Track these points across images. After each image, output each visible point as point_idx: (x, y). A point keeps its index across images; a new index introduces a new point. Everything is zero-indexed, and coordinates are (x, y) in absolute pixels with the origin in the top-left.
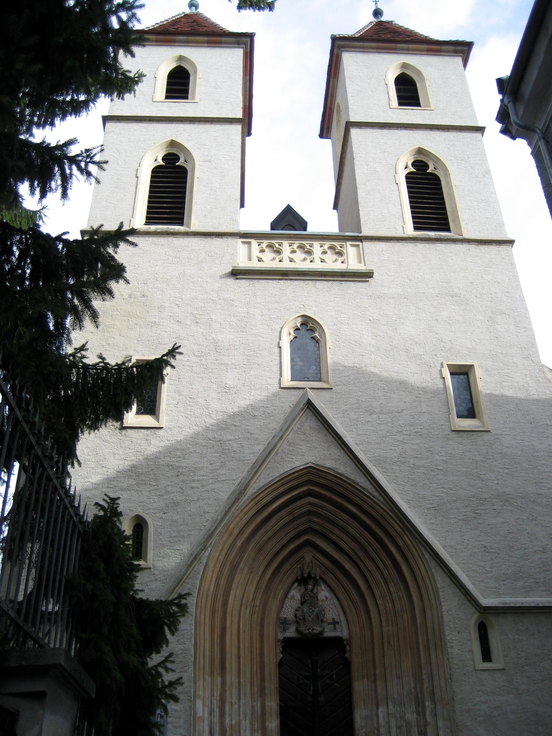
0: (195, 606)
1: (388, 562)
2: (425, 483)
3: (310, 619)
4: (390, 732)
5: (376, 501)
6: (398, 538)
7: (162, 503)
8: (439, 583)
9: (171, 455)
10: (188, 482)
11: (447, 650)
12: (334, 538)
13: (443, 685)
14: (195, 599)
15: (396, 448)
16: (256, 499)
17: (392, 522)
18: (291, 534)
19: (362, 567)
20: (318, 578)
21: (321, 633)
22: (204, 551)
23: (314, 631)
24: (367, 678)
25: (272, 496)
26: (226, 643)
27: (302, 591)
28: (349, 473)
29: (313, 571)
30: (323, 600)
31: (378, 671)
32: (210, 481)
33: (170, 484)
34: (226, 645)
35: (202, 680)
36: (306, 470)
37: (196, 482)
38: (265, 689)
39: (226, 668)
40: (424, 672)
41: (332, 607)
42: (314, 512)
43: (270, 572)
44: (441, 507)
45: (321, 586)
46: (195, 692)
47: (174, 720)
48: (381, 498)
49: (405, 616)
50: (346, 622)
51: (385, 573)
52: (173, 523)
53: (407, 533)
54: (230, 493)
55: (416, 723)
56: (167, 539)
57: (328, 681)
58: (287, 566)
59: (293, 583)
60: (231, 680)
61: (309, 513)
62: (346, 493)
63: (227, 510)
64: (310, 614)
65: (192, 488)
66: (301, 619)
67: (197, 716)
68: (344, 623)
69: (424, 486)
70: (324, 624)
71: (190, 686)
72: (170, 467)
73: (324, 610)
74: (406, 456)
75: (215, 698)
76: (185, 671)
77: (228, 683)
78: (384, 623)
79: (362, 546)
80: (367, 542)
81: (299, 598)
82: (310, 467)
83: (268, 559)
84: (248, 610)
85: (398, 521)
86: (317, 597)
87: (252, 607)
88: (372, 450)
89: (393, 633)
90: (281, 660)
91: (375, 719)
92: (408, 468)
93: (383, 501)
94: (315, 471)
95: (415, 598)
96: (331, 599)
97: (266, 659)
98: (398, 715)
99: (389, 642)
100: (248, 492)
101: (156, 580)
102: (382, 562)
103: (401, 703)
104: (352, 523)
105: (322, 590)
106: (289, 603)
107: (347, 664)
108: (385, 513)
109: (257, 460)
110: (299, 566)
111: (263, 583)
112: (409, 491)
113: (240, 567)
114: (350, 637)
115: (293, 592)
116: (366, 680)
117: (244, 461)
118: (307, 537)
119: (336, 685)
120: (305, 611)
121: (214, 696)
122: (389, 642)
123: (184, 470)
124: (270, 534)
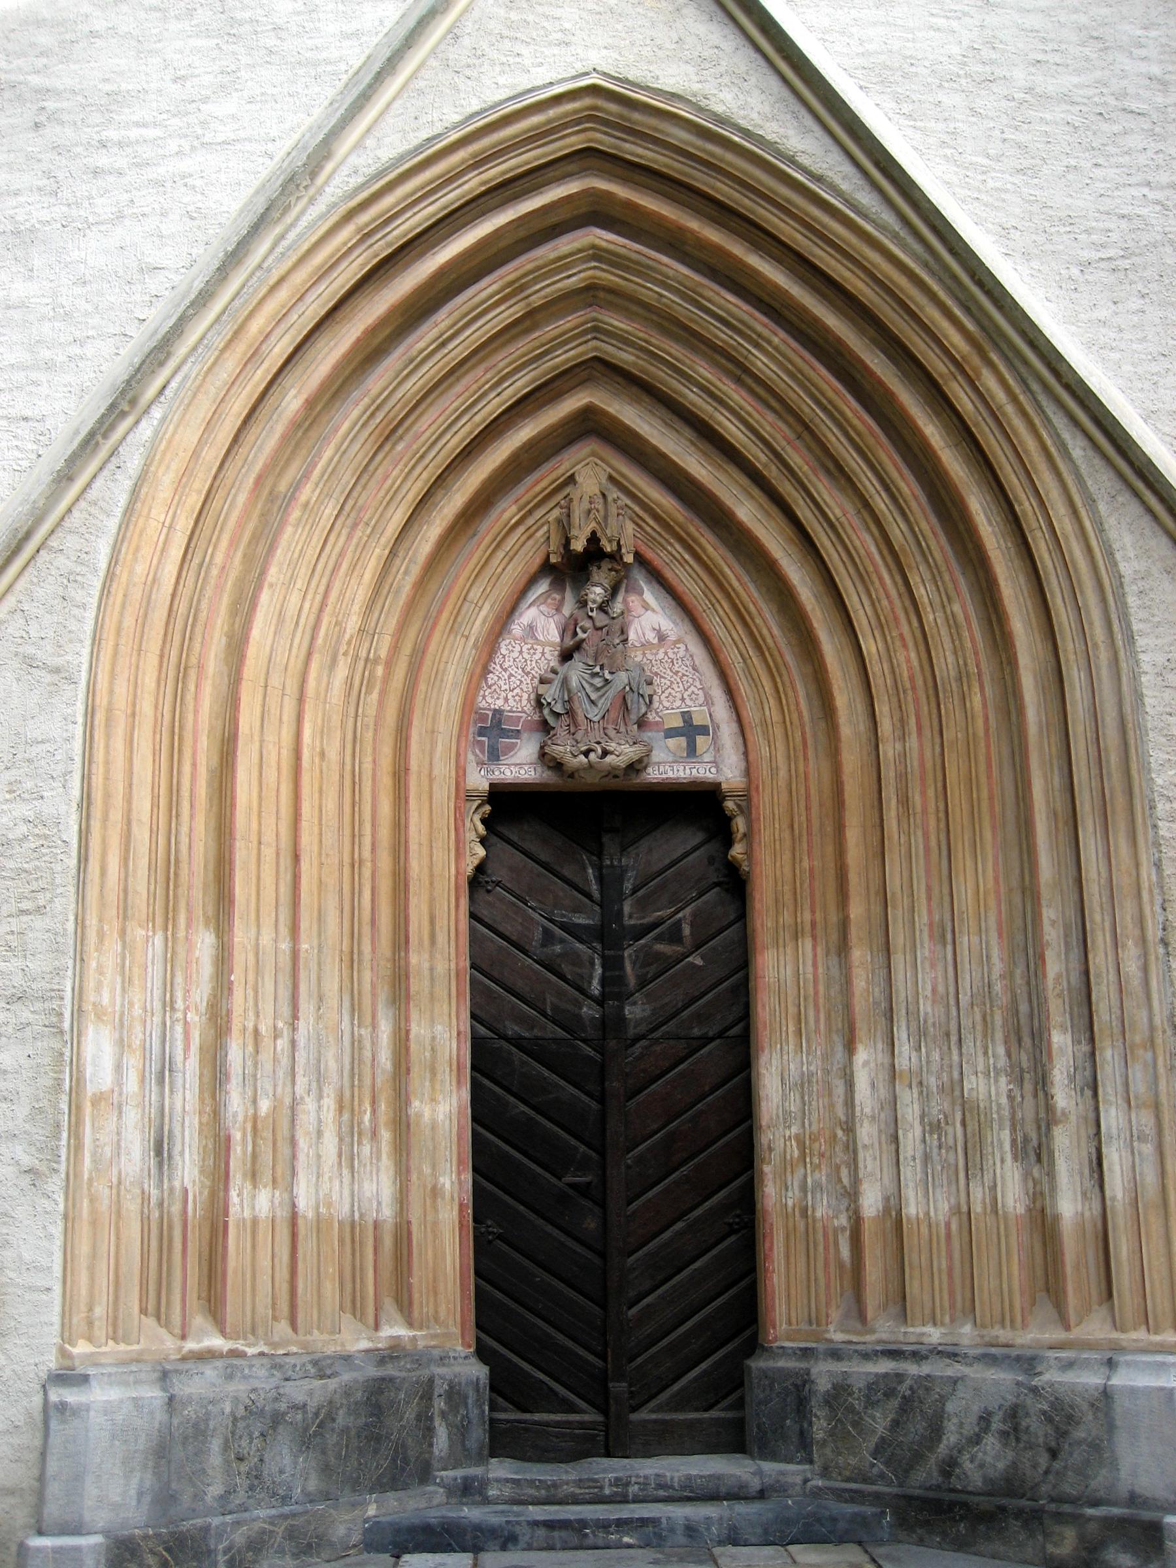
0: (88, 642)
1: (908, 486)
2: (1073, 162)
3: (594, 714)
4: (895, 1139)
5: (869, 228)
6: (955, 385)
10: (79, 149)
11: (1155, 826)
12: (692, 398)
13: (1131, 967)
14: (90, 615)
15: (954, 24)
16: (364, 218)
17: (932, 314)
18: (521, 384)
19: (804, 512)
20: (629, 558)
21: (636, 767)
24: (814, 938)
25: (431, 209)
28: (755, 116)
30: (646, 645)
31: (856, 910)
32: (173, 146)
34: (233, 806)
35: (113, 945)
36: (576, 105)
37: (115, 150)
38: (407, 977)
39: (232, 902)
40: (1049, 914)
42: (612, 291)
44: (1137, 260)
45: (641, 593)
46: (79, 993)
48: (888, 218)
49: (977, 699)
50: (734, 726)
51: (897, 531)
52: (12, 312)
53: (994, 357)
54: (251, 191)
55: (1006, 1113)
57: (660, 947)
58: (507, 510)
59: (532, 581)
60: (257, 945)
61: (590, 294)
63: (230, 249)
64: (594, 696)
65: (96, 172)
66: (557, 715)
67: (90, 1090)
68: (727, 732)
69: (1070, 177)
71: (58, 972)
73: (650, 683)
75: (179, 1015)
76: (39, 910)
77: (241, 958)
78: (886, 726)
79: (805, 429)
80: (824, 409)
81: (554, 635)
82: (594, 90)
83: (425, 475)
84: (342, 672)
85: (958, 312)
86: (623, 631)
87: (361, 664)
88: (854, 30)
89: (922, 764)
90: (480, 869)
91: (840, 1090)
92: (1004, 104)
93: (896, 226)
94: (613, 107)
96: (679, 641)
98: (933, 1080)
99: (905, 801)
102: (887, 489)
103: (948, 1035)
104: (766, 333)
105: (646, 607)
106: (516, 654)
108: (903, 281)
109: (368, 57)
110: (556, 513)
111: (406, 573)
112: (1006, 191)
114: (749, 782)
115: (529, 615)
116: (808, 943)
117: (316, 64)
119: (690, 959)
120: (574, 682)
121: (173, 1009)
122: (905, 801)
123: (65, 104)
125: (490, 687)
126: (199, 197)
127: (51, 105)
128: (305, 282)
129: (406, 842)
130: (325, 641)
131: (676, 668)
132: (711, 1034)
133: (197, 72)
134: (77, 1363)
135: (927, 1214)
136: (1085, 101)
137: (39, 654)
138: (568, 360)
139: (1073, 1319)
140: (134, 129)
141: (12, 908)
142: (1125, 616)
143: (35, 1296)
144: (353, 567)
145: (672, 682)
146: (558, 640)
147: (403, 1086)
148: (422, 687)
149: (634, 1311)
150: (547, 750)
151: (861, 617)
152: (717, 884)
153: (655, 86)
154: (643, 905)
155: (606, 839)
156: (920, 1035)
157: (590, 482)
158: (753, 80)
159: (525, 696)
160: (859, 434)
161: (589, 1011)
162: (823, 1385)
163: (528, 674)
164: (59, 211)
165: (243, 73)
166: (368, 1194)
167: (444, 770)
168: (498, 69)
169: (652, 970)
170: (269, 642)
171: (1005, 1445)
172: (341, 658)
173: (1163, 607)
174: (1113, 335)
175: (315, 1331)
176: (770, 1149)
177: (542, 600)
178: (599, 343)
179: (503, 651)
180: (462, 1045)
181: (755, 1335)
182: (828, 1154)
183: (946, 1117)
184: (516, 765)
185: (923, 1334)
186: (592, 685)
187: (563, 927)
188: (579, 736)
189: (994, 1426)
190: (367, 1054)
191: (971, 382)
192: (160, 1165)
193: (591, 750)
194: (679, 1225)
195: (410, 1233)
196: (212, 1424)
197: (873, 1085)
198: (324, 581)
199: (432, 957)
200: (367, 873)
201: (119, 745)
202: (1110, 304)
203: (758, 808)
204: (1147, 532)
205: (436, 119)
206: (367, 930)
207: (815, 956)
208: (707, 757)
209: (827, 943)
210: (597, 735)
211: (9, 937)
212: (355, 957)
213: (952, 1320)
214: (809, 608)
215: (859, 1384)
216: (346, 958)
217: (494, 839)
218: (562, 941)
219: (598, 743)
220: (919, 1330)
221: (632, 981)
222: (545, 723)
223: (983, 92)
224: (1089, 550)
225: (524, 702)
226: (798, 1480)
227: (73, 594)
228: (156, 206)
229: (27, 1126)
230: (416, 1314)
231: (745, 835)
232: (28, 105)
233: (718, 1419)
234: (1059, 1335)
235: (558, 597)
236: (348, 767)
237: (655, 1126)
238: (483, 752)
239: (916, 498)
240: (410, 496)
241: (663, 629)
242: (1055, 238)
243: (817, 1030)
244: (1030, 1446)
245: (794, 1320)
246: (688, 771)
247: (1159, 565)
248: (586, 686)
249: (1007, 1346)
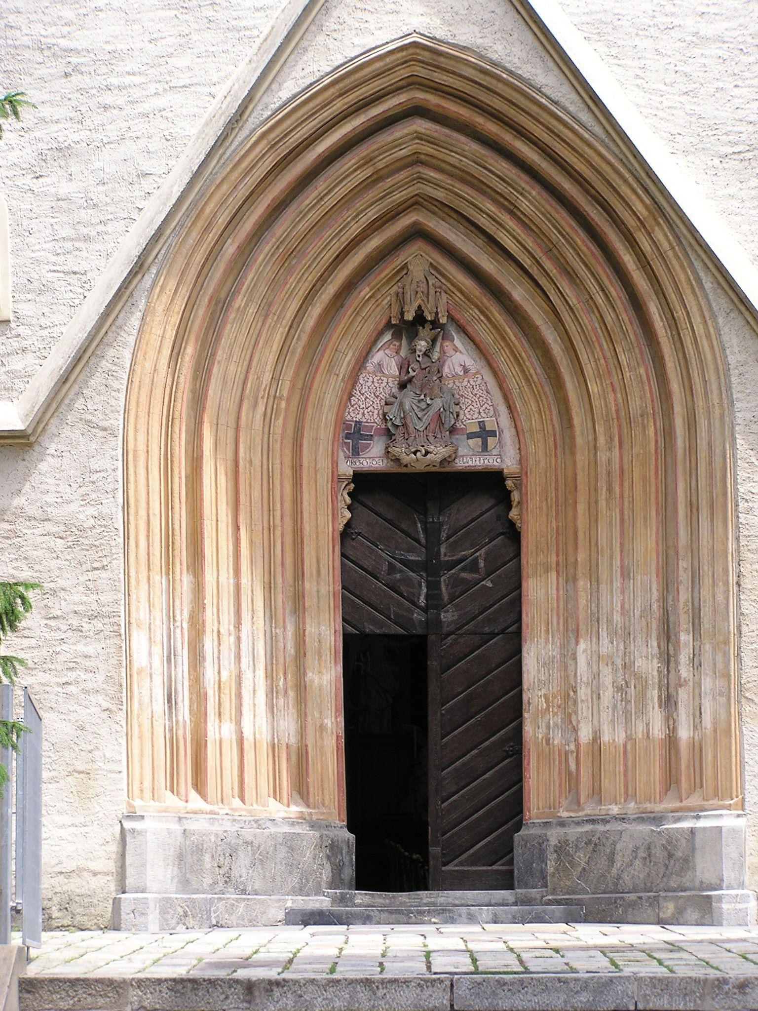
1: (616, 291)
2: (721, 85)
3: (420, 426)
7: (29, 151)
8: (733, 353)
9: (45, 19)
10: (94, 91)
11: (738, 516)
12: (482, 221)
14: (122, 396)
16: (272, 136)
17: (624, 190)
18: (372, 214)
22: (140, 276)
23: (429, 456)
24: (558, 573)
25: (313, 123)
26: (202, 495)
27: (403, 353)
28: (516, 60)
30: (455, 376)
33: (47, 97)
35: (144, 586)
37: (116, 92)
39: (203, 557)
43: (316, 311)
47: (83, 677)
48: (597, 130)
52: (61, 203)
56: (46, 246)
57: (464, 575)
58: (365, 291)
59: (381, 333)
61: (416, 160)
62: (512, 113)
65: (106, 108)
68: (508, 435)
69: (717, 95)
70: (460, 438)
72: (46, 53)
74: (674, 10)
78: (602, 441)
80: (564, 237)
82: (414, 44)
84: (261, 409)
90: (348, 525)
92: (680, 45)
95: (675, 386)
96: (477, 373)
97: (308, 528)
100: (249, 116)
101: (24, 350)
102: (603, 290)
105: (456, 350)
106: (369, 384)
107: (514, 535)
110: (395, 288)
111: (298, 339)
112: (676, 108)
113: (237, 306)
115: (378, 357)
116: (554, 575)
118: (414, 219)
120: (407, 407)
124: (313, 216)
125: (352, 406)
126: (171, 125)
127: (74, 60)
128: (237, 178)
129: (302, 512)
130: (250, 391)
131: (475, 392)
132: (496, 631)
133: (163, 35)
134: (137, 810)
135: (614, 740)
136: (732, 40)
137: (94, 419)
138: (401, 197)
139: (684, 795)
140: (127, 76)
141: (88, 566)
142: (729, 388)
143: (114, 775)
144: (266, 342)
146: (398, 373)
147: (302, 664)
148: (310, 411)
149: (445, 804)
150: (390, 450)
151: (589, 370)
152: (502, 534)
153: (453, 41)
154: (453, 547)
155: (429, 504)
156: (613, 634)
157: (418, 270)
158: (516, 36)
159: (376, 412)
160: (585, 256)
161: (418, 616)
162: (553, 841)
163: (377, 397)
164: (84, 134)
165: (193, 35)
166: (282, 728)
167: (324, 464)
168: (354, 32)
169: (458, 590)
170: (219, 396)
171: (644, 865)
172: (260, 400)
173: (753, 383)
174: (738, 205)
175: (255, 805)
176: (529, 703)
177: (386, 346)
178: (422, 185)
179: (361, 381)
180: (338, 638)
181: (521, 820)
182: (563, 706)
183: (626, 683)
185: (609, 809)
187: (402, 562)
188: (410, 442)
189: (639, 855)
190: (281, 645)
191: (649, 234)
192: (170, 708)
193: (418, 451)
194: (475, 751)
195: (307, 753)
196: (205, 846)
197: (588, 664)
198: (249, 352)
199: (318, 583)
200: (278, 534)
201: (142, 472)
202: (738, 183)
203: (526, 487)
204: (748, 336)
205: (315, 70)
206: (279, 569)
207: (558, 583)
208: (494, 452)
209: (567, 575)
210: (422, 440)
211: (88, 583)
212: (272, 585)
213: (625, 801)
214: (558, 359)
215: (572, 839)
216: (267, 586)
217: (357, 505)
218: (401, 571)
220: (607, 807)
221: (446, 597)
222: (388, 430)
223: (665, 37)
224: (712, 347)
225: (375, 416)
226: (538, 896)
227: (112, 383)
228: (145, 131)
229: (104, 686)
230: (311, 800)
231: (519, 502)
232: (60, 60)
233: (496, 871)
234: (678, 804)
235: (397, 344)
236: (265, 467)
237: (460, 690)
238: (348, 450)
239: (620, 298)
240: (301, 292)
242: (706, 140)
243: (558, 629)
244: (655, 864)
245: (541, 806)
246: (482, 461)
247: (753, 357)
248: (415, 408)
249: (651, 812)
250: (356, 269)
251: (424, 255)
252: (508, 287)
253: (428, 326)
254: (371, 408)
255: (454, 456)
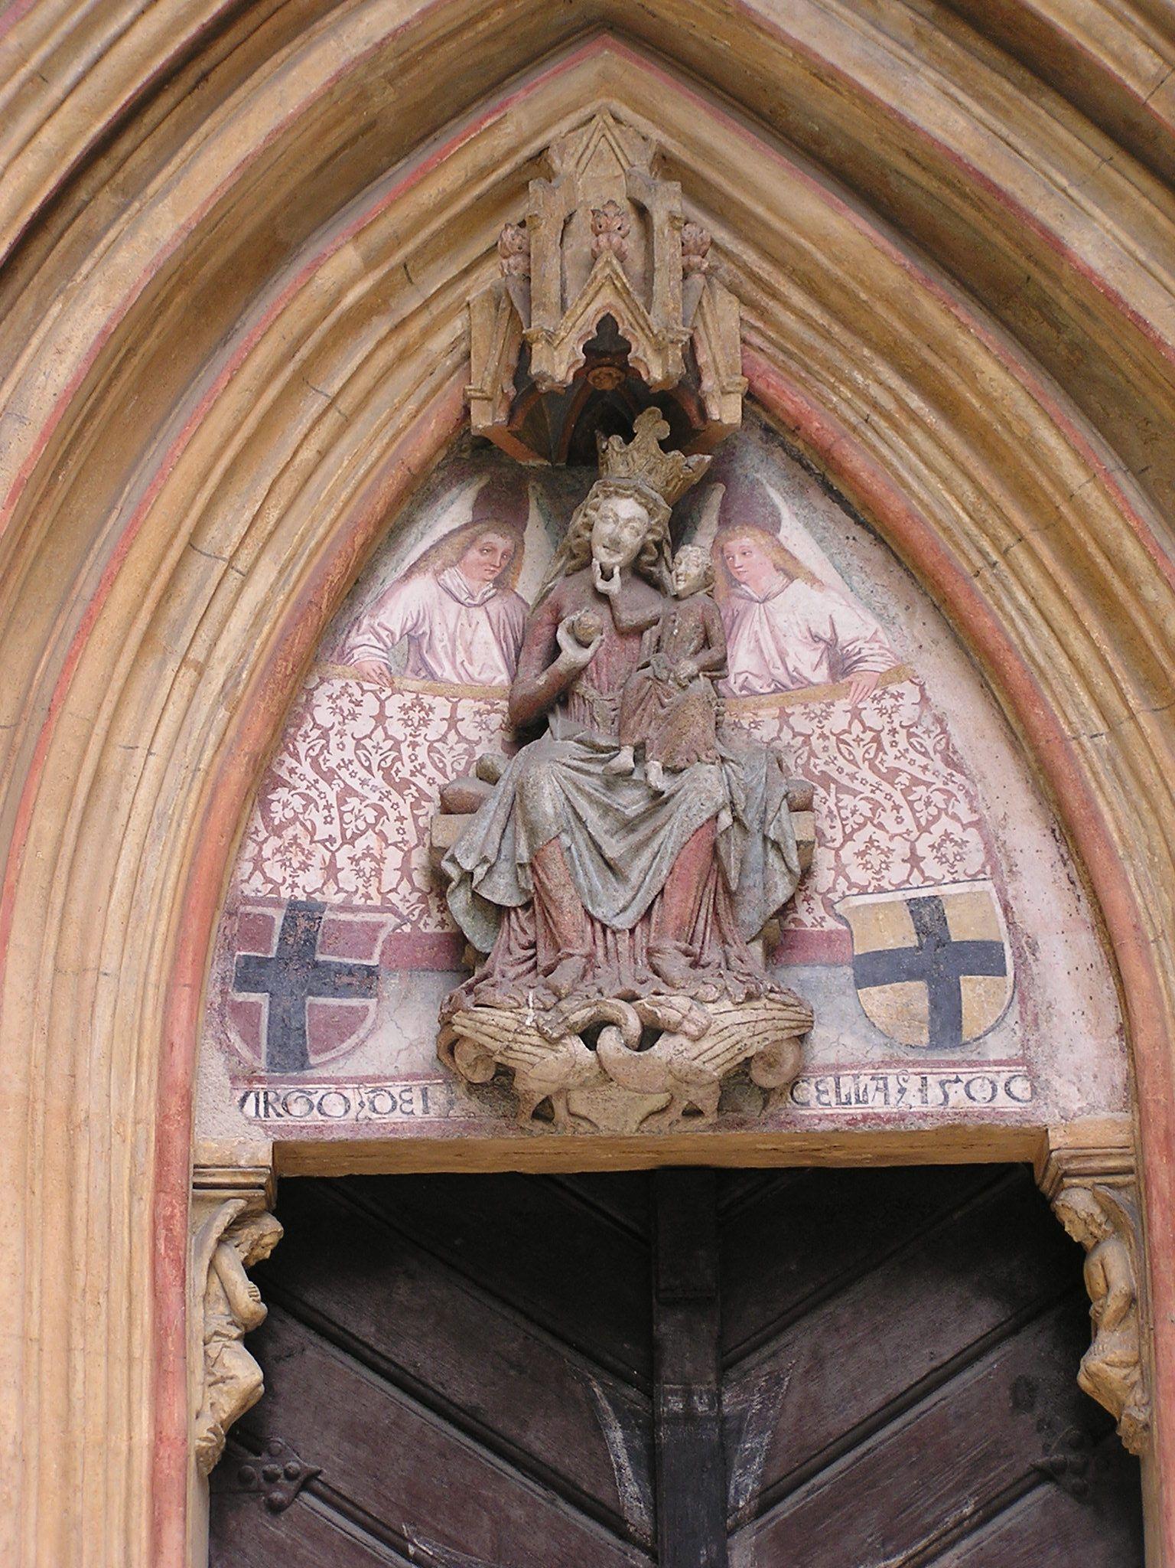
23: (663, 1048)
29: (655, 320)
41: (912, 766)
45: (771, 525)
50: (1087, 942)
64: (614, 848)
66: (498, 913)
96: (899, 672)
105: (790, 569)
106: (362, 726)
110: (489, 276)
125: (277, 831)
145: (876, 806)
146: (503, 677)
152: (1045, 1475)
155: (665, 1329)
159: (394, 857)
177: (449, 552)
179: (323, 715)
184: (361, 1081)
186: (606, 810)
188: (563, 977)
208: (997, 1047)
210: (628, 973)
219: (631, 998)
222: (457, 941)
225: (390, 878)
231: (1132, 1300)
238: (252, 1041)
241: (844, 636)
246: (935, 1093)
248: (590, 814)
250: (282, 131)
251: (625, 112)
252: (1045, 210)
253: (651, 427)
254: (370, 840)
255: (789, 1054)
